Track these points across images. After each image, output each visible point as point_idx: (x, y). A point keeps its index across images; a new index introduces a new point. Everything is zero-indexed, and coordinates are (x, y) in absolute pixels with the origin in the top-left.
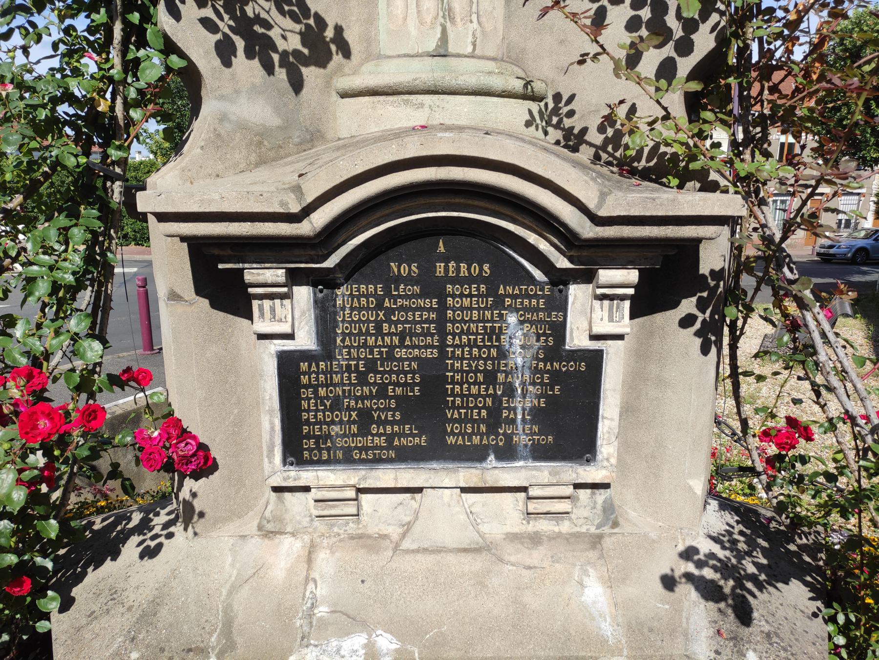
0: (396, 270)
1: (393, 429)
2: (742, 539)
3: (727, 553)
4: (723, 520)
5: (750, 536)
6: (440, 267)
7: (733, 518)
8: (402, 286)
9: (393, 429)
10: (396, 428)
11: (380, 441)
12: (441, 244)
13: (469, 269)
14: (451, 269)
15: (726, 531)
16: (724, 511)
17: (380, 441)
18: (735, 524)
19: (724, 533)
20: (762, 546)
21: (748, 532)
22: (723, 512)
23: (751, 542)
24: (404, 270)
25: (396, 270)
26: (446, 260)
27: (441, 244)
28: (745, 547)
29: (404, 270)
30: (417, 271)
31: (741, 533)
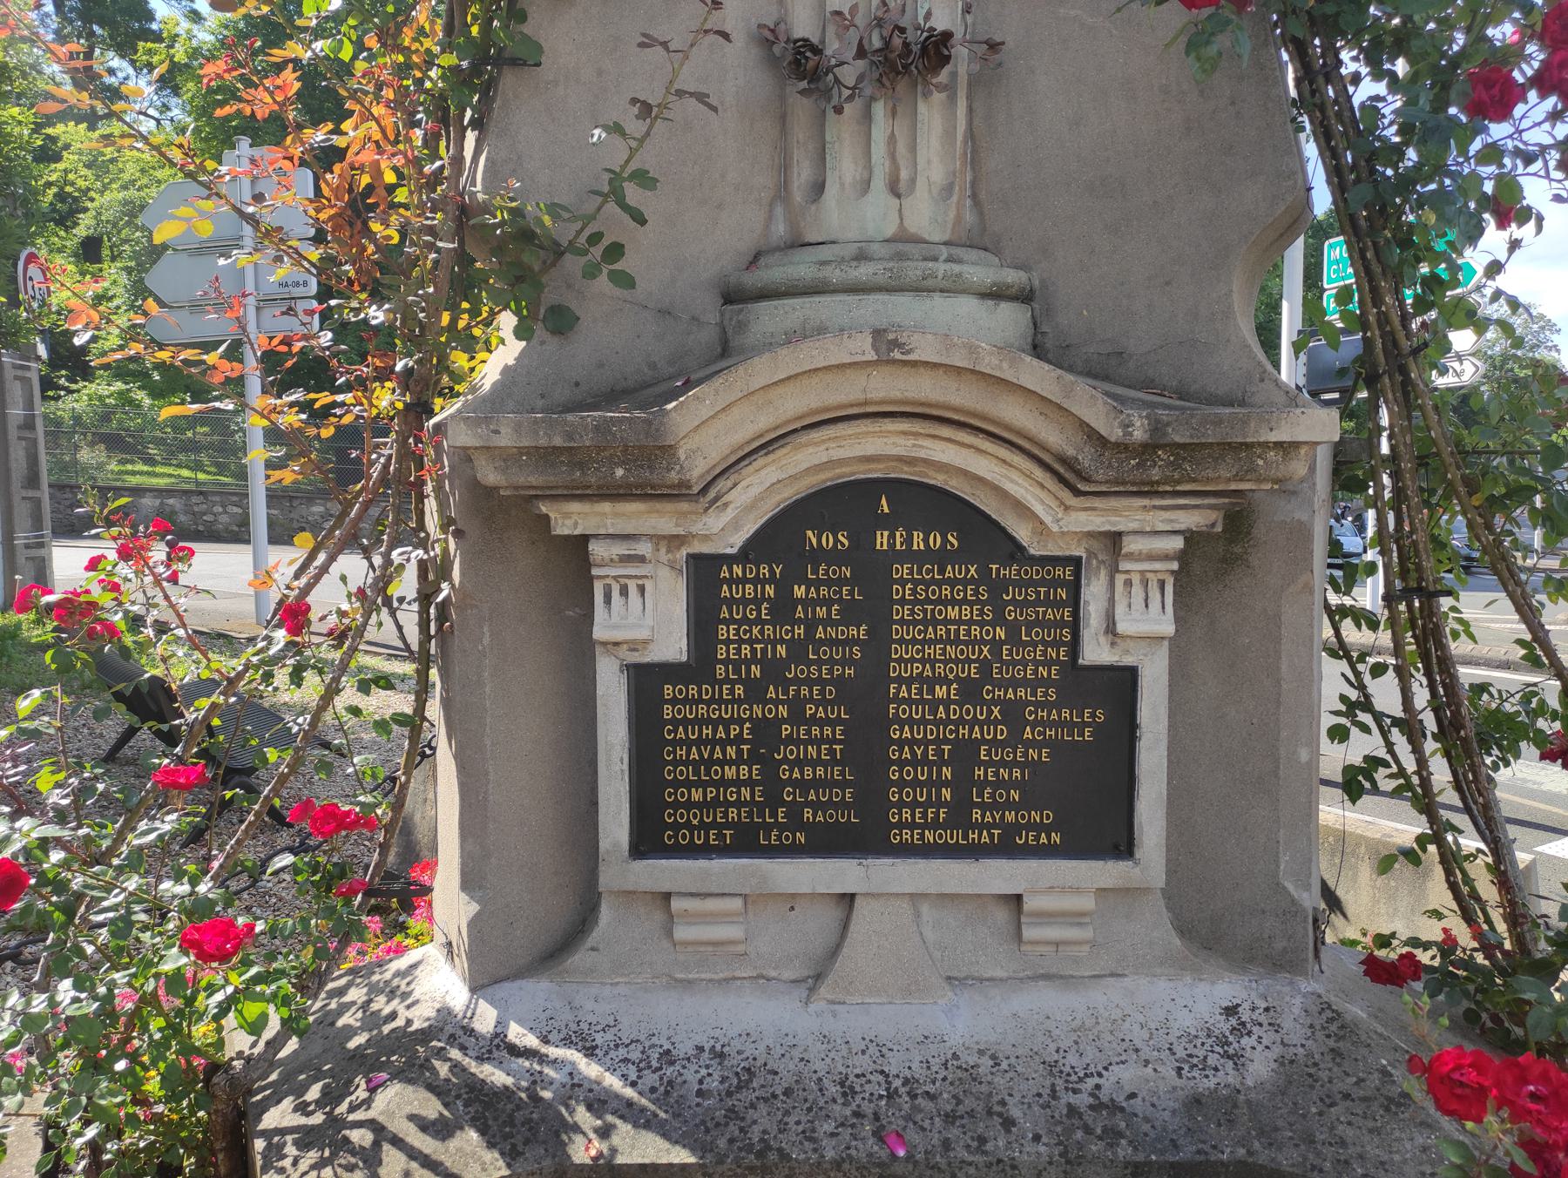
0: (814, 541)
1: (814, 772)
2: (387, 1010)
3: (388, 976)
4: (427, 997)
5: (379, 1027)
6: (882, 540)
7: (419, 1018)
8: (823, 566)
9: (814, 772)
10: (820, 771)
11: (912, 836)
12: (884, 502)
13: (926, 541)
14: (898, 540)
15: (411, 993)
16: (438, 1011)
17: (912, 836)
18: (410, 1014)
19: (412, 986)
20: (356, 1034)
21: (386, 1029)
22: (438, 1006)
23: (373, 1020)
24: (828, 541)
25: (814, 541)
26: (890, 523)
27: (884, 502)
28: (374, 1007)
29: (828, 541)
30: (846, 542)
31: (393, 1016)
